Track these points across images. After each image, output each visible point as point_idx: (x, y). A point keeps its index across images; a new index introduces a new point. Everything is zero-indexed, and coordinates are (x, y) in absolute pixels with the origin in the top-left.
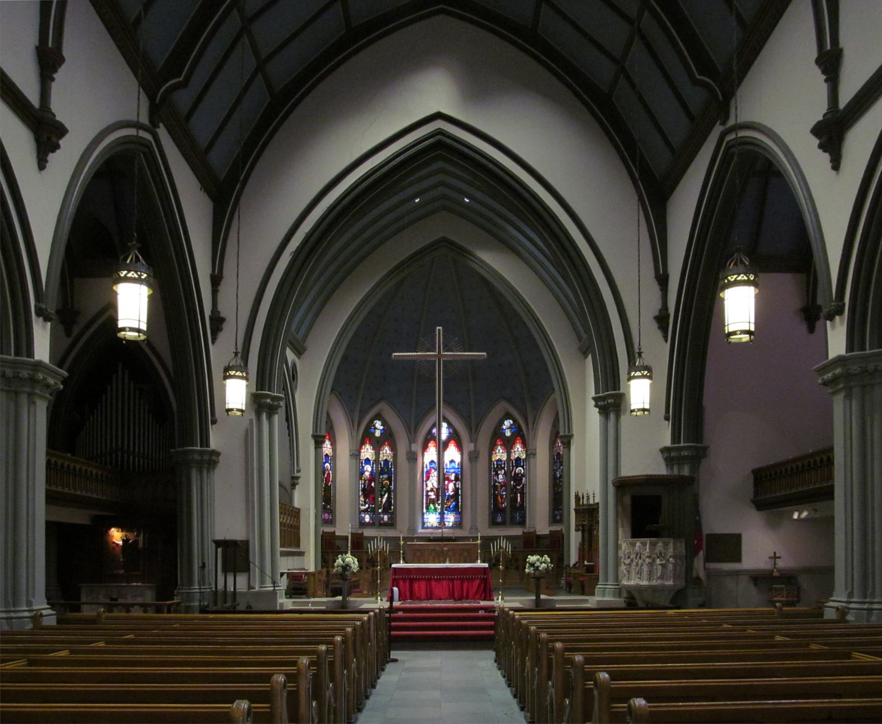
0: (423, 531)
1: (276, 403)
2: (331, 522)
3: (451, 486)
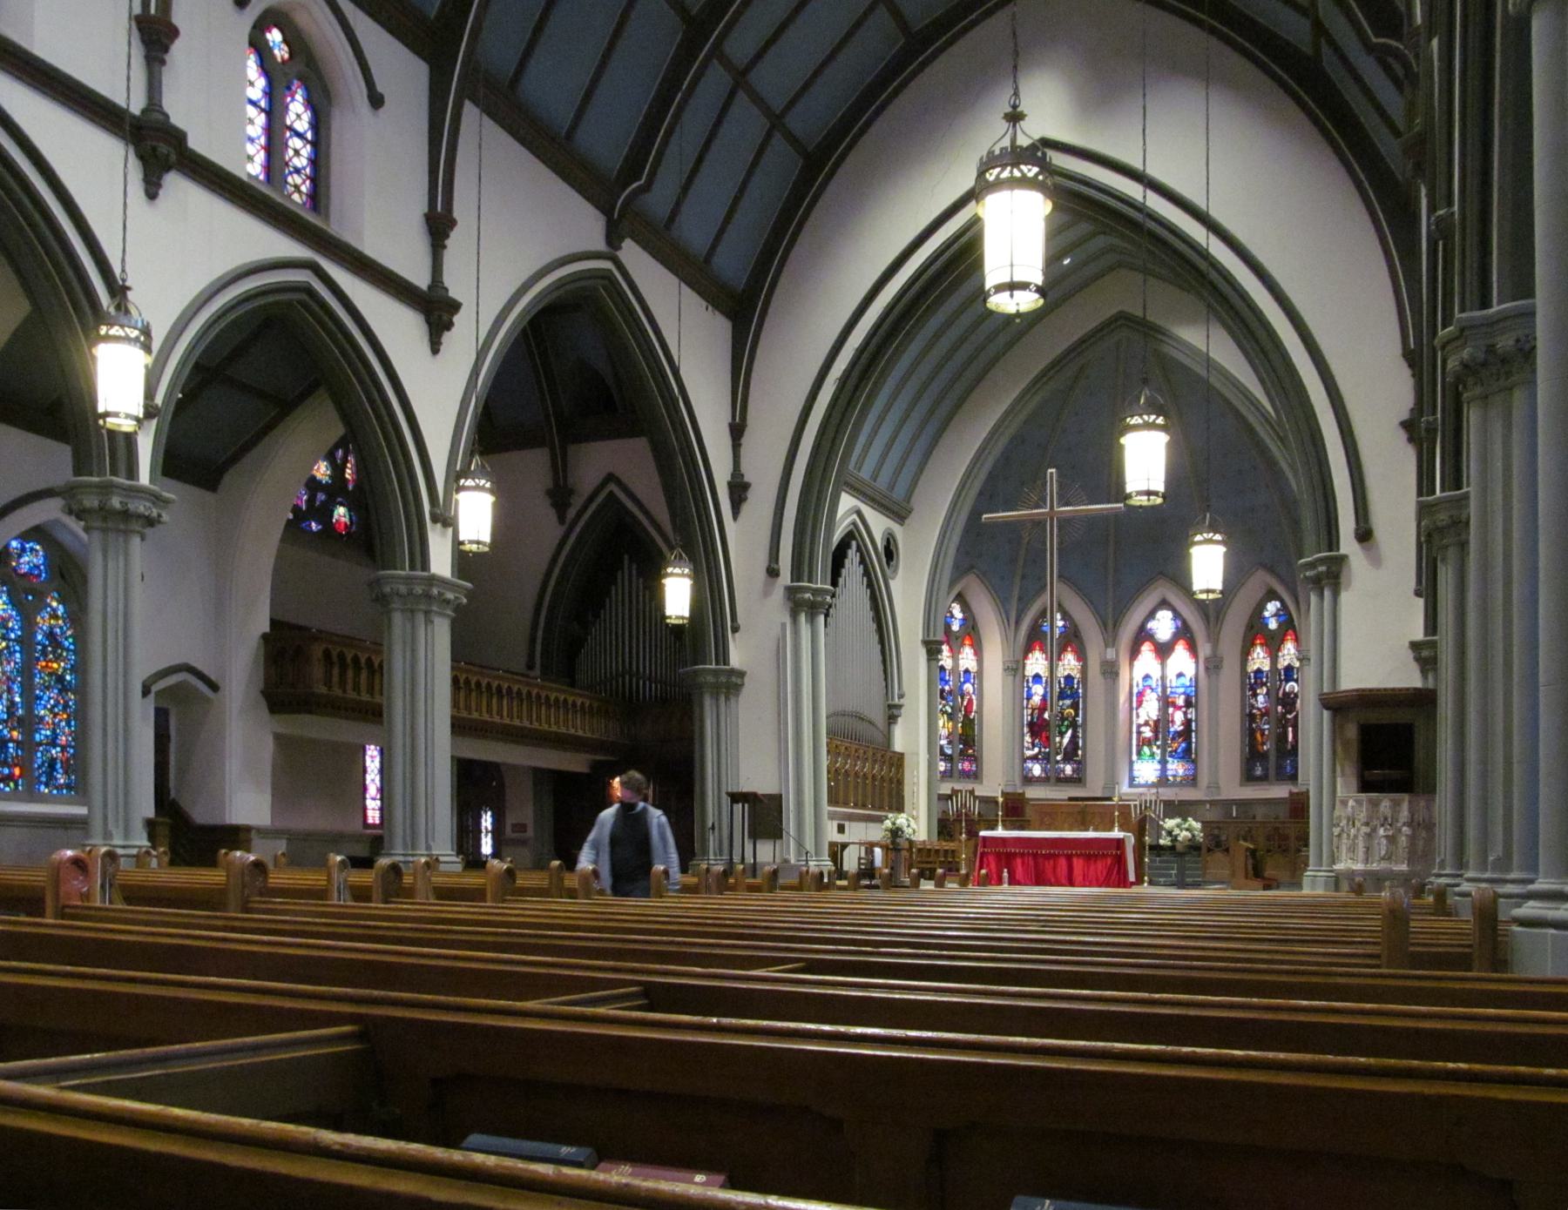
1: (819, 599)
3: (1179, 717)
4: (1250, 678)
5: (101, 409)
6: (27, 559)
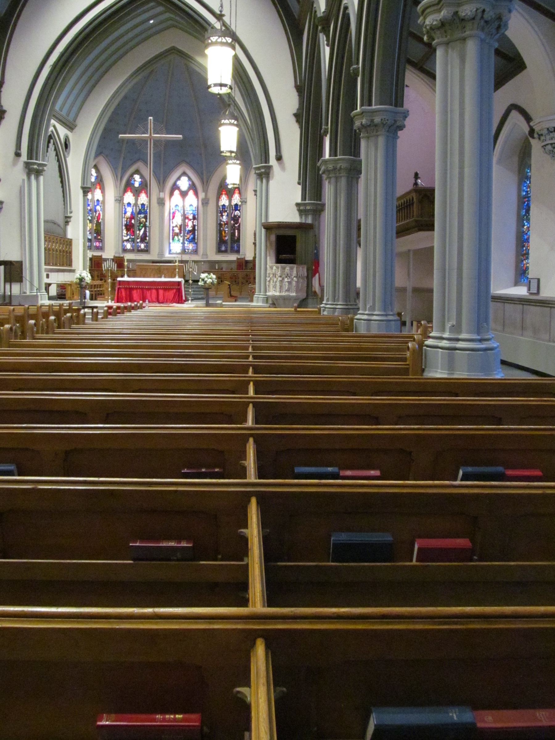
1: (41, 168)
3: (190, 224)
4: (220, 208)
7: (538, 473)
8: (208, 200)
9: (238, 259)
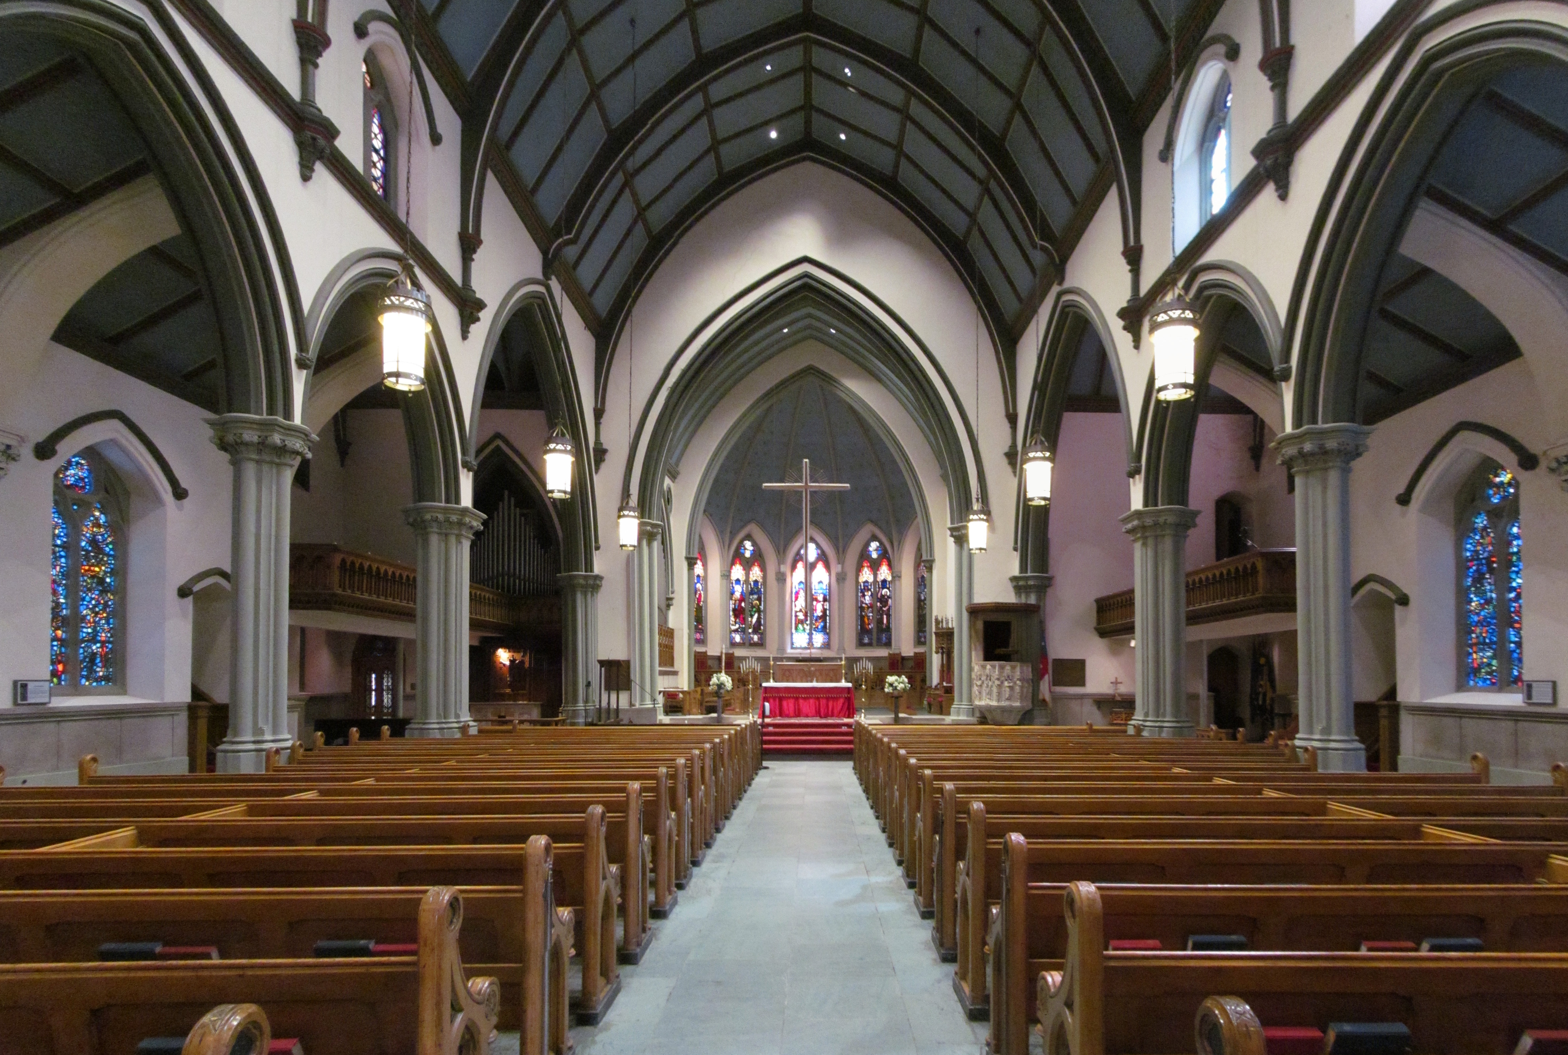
0: (793, 651)
1: (655, 530)
2: (701, 642)
5: (387, 369)
6: (72, 472)
7: (1241, 938)
8: (846, 575)
9: (890, 654)
